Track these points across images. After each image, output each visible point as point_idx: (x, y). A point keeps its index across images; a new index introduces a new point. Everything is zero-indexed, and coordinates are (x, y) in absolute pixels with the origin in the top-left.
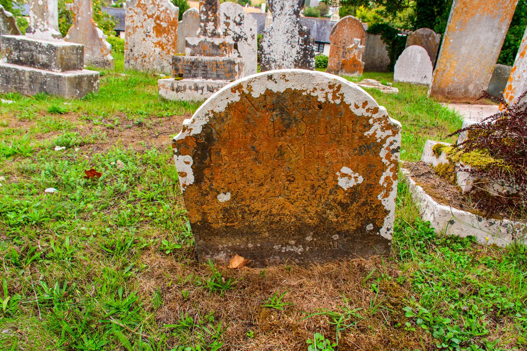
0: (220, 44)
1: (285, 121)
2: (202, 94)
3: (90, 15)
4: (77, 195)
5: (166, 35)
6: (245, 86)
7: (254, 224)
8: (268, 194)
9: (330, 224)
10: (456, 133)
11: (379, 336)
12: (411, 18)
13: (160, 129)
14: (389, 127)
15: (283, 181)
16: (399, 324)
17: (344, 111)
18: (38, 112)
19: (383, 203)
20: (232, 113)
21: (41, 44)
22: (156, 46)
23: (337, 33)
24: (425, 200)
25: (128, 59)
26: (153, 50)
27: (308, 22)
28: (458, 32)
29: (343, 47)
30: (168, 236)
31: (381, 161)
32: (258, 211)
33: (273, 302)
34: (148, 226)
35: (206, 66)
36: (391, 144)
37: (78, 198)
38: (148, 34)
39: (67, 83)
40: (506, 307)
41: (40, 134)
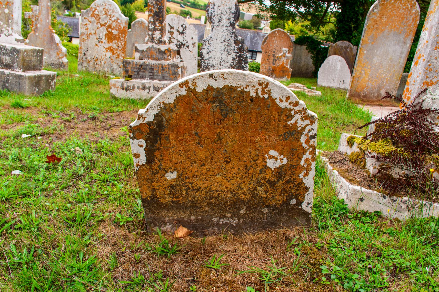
0: (166, 50)
1: (223, 111)
2: (149, 93)
3: (48, 23)
4: (40, 176)
5: (116, 41)
6: (191, 83)
7: (196, 199)
8: (208, 173)
9: (260, 199)
10: (364, 126)
11: (300, 289)
12: (332, 32)
13: (111, 123)
14: (308, 117)
15: (221, 162)
16: (317, 279)
17: (271, 104)
18: (2, 106)
19: (304, 181)
20: (179, 104)
21: (5, 47)
22: (107, 51)
23: (268, 43)
24: (340, 182)
25: (81, 61)
26: (104, 54)
27: (243, 33)
28: (370, 44)
29: (274, 55)
30: (121, 211)
31: (301, 146)
32: (200, 188)
33: (212, 263)
34: (104, 203)
35: (153, 69)
36: (310, 131)
37: (41, 179)
38: (100, 40)
39: (27, 82)
40: (404, 265)
41: (4, 125)
